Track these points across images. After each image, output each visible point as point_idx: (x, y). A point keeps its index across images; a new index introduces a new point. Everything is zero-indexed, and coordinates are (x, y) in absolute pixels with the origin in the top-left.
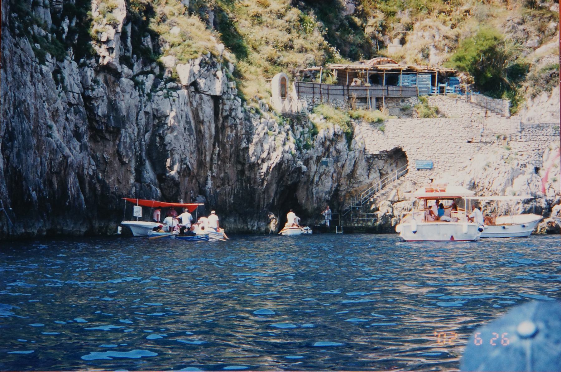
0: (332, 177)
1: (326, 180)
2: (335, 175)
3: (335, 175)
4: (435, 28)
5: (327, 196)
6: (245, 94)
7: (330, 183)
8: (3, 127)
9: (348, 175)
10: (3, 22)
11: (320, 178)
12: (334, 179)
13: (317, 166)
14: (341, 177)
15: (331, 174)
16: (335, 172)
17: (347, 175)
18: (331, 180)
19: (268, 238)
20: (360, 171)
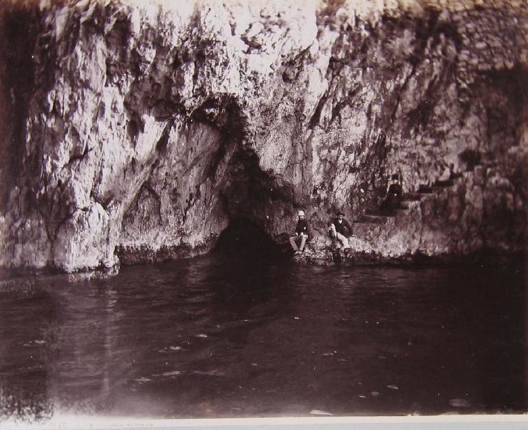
0: (369, 114)
1: (353, 120)
2: (376, 108)
3: (376, 108)
4: (237, 58)
5: (352, 156)
6: (61, 413)
7: (363, 127)
8: (3, 10)
9: (412, 114)
10: (45, 173)
11: (336, 112)
12: (374, 118)
13: (331, 84)
14: (393, 117)
15: (366, 105)
16: (377, 101)
17: (409, 114)
18: (364, 119)
19: (459, 116)
20: (443, 107)
